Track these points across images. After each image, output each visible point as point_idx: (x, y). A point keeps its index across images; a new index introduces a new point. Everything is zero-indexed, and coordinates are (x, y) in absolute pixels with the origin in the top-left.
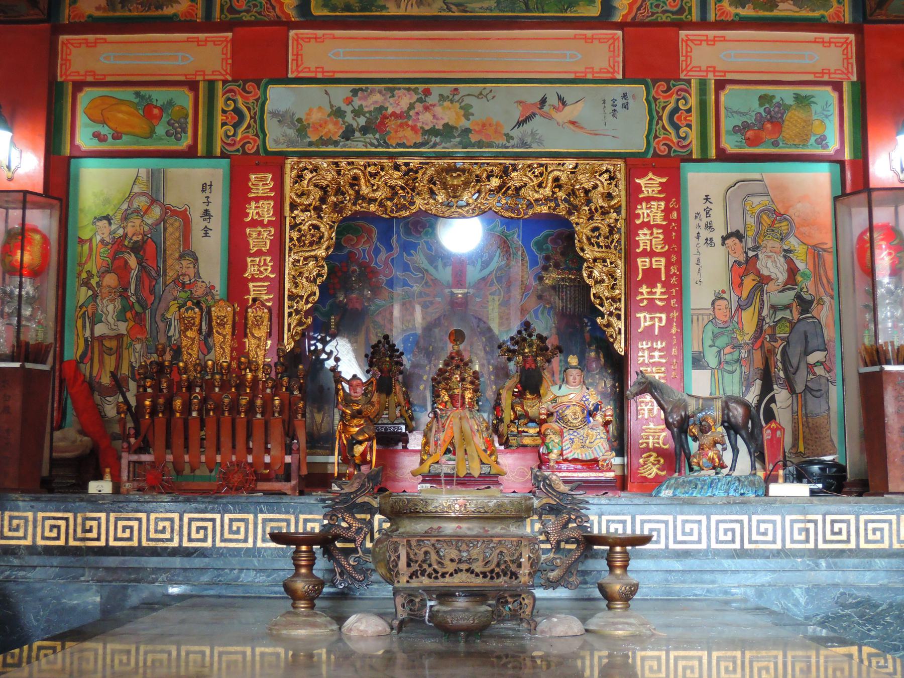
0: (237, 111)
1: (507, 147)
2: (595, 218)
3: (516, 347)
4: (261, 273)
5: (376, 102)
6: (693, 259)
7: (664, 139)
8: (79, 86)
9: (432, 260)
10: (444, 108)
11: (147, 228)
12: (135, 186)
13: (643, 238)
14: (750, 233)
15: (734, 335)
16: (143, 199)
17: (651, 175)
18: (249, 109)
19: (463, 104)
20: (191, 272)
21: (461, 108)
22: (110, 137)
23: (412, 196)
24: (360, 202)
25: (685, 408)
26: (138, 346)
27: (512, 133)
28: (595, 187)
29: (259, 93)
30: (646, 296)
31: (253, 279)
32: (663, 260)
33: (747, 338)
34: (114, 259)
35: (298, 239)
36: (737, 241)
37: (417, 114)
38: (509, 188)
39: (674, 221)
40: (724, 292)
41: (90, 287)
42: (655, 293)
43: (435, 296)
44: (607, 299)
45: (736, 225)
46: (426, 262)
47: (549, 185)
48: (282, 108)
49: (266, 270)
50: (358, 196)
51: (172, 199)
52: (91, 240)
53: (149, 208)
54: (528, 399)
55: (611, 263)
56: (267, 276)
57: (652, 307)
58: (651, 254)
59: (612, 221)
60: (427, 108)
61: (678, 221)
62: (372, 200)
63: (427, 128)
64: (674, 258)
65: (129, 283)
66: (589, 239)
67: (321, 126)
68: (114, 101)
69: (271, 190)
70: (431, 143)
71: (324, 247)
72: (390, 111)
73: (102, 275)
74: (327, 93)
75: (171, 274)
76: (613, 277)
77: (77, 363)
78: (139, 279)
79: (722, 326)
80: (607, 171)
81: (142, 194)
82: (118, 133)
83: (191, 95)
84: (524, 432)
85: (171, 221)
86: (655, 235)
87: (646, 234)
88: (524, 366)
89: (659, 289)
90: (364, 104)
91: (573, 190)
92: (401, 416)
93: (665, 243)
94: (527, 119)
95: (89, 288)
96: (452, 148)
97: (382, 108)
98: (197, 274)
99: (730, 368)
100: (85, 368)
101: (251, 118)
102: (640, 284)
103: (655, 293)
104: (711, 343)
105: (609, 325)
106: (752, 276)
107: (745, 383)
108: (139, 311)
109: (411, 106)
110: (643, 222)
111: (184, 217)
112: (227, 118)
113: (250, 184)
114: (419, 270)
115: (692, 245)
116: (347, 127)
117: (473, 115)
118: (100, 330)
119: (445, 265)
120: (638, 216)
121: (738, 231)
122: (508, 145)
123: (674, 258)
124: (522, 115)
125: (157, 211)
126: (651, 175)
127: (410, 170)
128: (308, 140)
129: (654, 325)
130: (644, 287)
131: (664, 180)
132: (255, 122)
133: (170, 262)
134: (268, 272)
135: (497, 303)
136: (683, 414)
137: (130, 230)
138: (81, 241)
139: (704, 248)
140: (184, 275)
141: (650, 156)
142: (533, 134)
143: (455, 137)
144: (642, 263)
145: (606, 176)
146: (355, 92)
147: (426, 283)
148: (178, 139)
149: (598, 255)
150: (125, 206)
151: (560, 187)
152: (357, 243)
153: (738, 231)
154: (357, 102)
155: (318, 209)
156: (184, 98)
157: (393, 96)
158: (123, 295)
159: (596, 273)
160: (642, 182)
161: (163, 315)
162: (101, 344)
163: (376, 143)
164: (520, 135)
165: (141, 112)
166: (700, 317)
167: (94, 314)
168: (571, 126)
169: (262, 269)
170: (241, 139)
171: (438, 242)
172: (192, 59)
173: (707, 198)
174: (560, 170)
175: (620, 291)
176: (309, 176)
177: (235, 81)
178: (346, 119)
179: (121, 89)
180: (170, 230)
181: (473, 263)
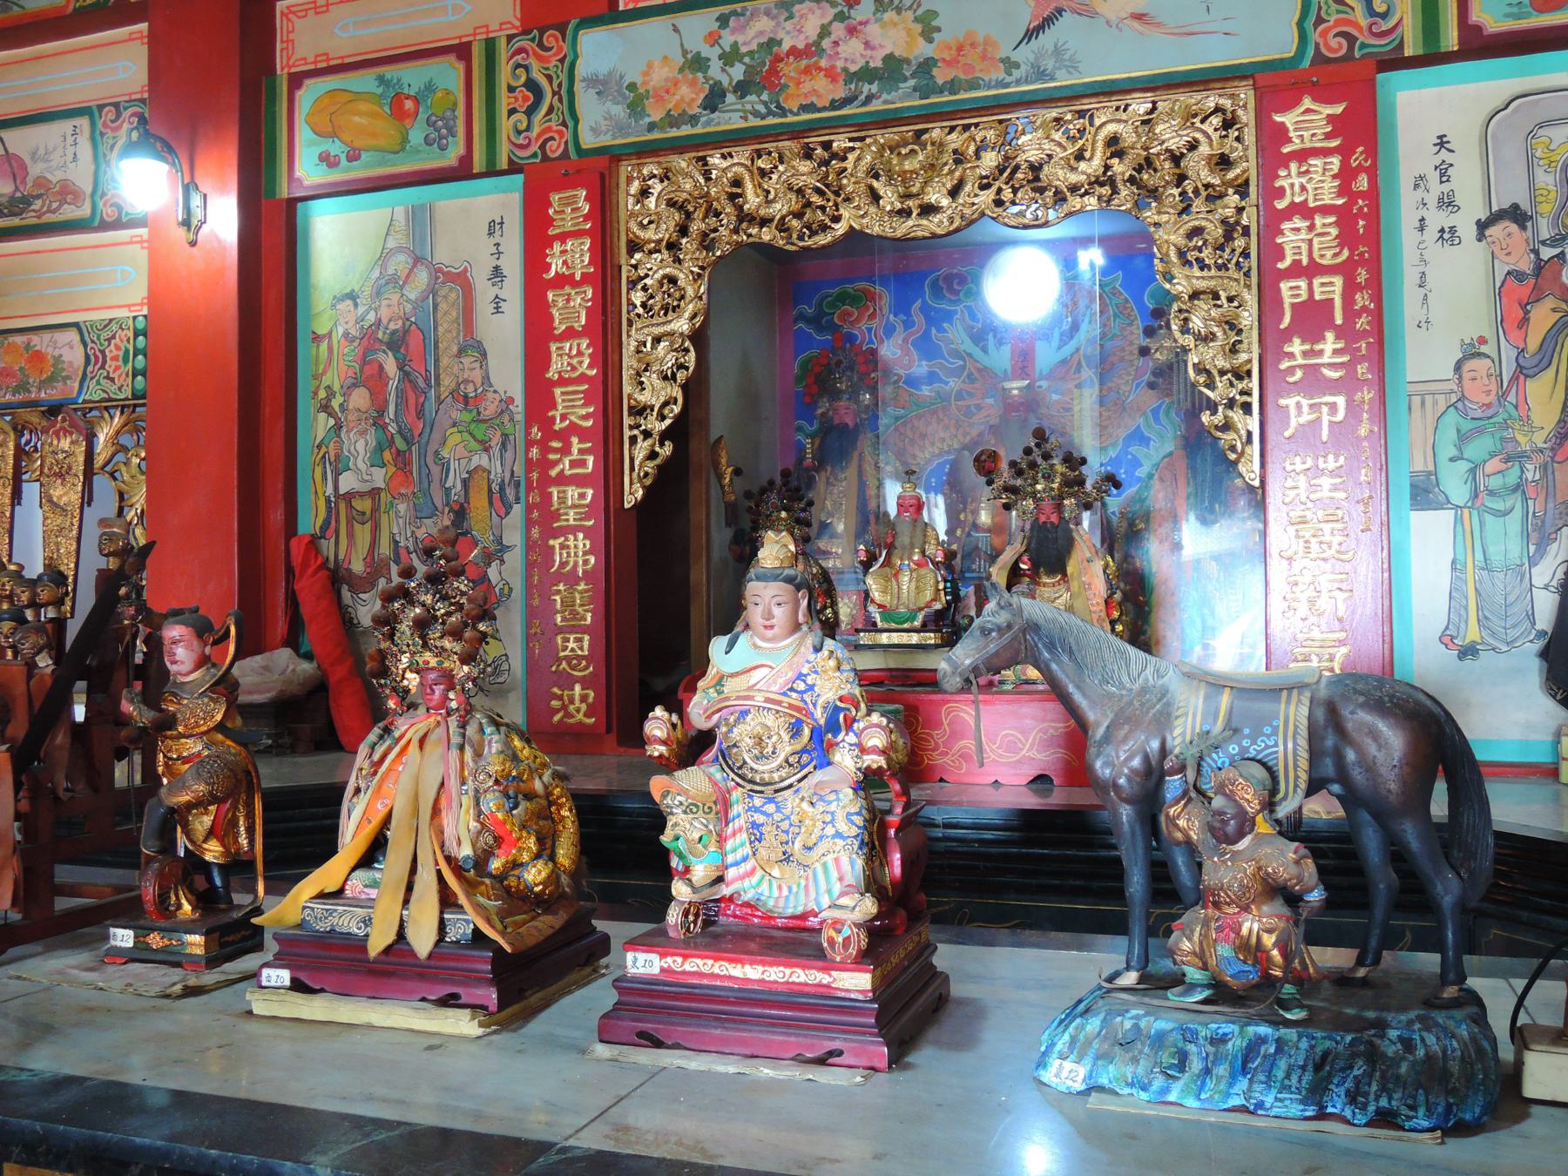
0: (531, 85)
1: (1007, 85)
2: (1194, 209)
3: (1019, 482)
4: (574, 369)
5: (761, 33)
6: (1410, 276)
7: (1338, 23)
8: (296, 81)
9: (978, 338)
10: (884, 26)
11: (409, 307)
12: (390, 238)
13: (1293, 239)
14: (1545, 208)
15: (1508, 434)
16: (402, 258)
17: (1307, 102)
18: (549, 78)
19: (919, 12)
20: (477, 376)
21: (916, 20)
22: (343, 157)
23: (836, 205)
24: (744, 225)
25: (1164, 720)
26: (402, 508)
27: (1016, 56)
28: (1193, 146)
29: (566, 47)
30: (1300, 361)
31: (562, 381)
32: (1338, 281)
33: (1539, 439)
34: (364, 362)
35: (644, 305)
36: (1514, 227)
37: (836, 43)
38: (1017, 168)
39: (1361, 194)
40: (1482, 341)
41: (331, 414)
42: (1321, 352)
44: (1222, 373)
45: (1512, 192)
47: (1099, 154)
48: (603, 70)
49: (581, 363)
50: (744, 217)
51: (444, 255)
52: (330, 334)
53: (411, 270)
54: (1045, 585)
55: (1230, 299)
56: (583, 374)
57: (1314, 382)
58: (1311, 270)
59: (1229, 212)
60: (852, 31)
61: (1373, 195)
62: (765, 222)
63: (853, 68)
64: (1362, 275)
65: (386, 402)
66: (1181, 254)
67: (667, 92)
68: (347, 97)
69: (586, 218)
70: (863, 97)
71: (687, 315)
72: (786, 46)
73: (347, 392)
74: (676, 30)
75: (447, 382)
76: (1232, 326)
77: (313, 541)
78: (401, 395)
79: (1479, 414)
80: (1218, 110)
81: (400, 249)
82: (354, 149)
83: (461, 66)
85: (442, 292)
86: (1319, 230)
87: (1298, 230)
89: (1330, 343)
90: (740, 39)
91: (1147, 159)
93: (1341, 246)
94: (1047, 22)
95: (330, 415)
96: (901, 99)
97: (773, 42)
98: (486, 378)
99: (1499, 505)
100: (328, 547)
101: (554, 94)
102: (1287, 336)
103: (1321, 352)
104: (1453, 452)
105: (1227, 426)
106: (1550, 302)
107: (1534, 536)
108: (404, 453)
109: (825, 31)
110: (1293, 203)
111: (462, 280)
112: (516, 99)
113: (551, 211)
114: (957, 354)
115: (1409, 245)
116: (712, 88)
117: (939, 30)
118: (348, 482)
119: (1000, 343)
120: (1281, 193)
121: (1515, 207)
122: (1009, 79)
123: (1362, 275)
124: (1034, 17)
125: (422, 277)
126: (1307, 102)
127: (834, 156)
128: (647, 120)
129: (1318, 420)
130: (1297, 341)
131: (1338, 109)
132: (560, 100)
133: (444, 361)
134: (585, 367)
136: (1155, 745)
137: (384, 313)
138: (317, 338)
139: (1435, 251)
140: (466, 381)
141: (1306, 63)
142: (1058, 52)
143: (905, 80)
144: (1291, 291)
145: (1216, 121)
146: (723, 21)
147: (969, 376)
148: (443, 148)
149: (1202, 285)
150: (376, 274)
151: (1120, 154)
152: (858, 320)
153: (1515, 207)
154: (727, 39)
155: (672, 246)
156: (448, 75)
157: (791, 17)
158: (378, 423)
159: (1196, 323)
160: (1287, 119)
161: (437, 453)
162: (350, 507)
163: (763, 110)
164: (1032, 58)
165: (387, 109)
166: (1429, 399)
167: (337, 456)
168: (1136, 24)
169: (575, 361)
170: (539, 136)
172: (468, 8)
173: (1442, 142)
174: (1119, 121)
175: (1250, 354)
176: (656, 187)
177: (526, 32)
178: (711, 73)
179: (342, 76)
180: (443, 307)
181: (1047, 337)
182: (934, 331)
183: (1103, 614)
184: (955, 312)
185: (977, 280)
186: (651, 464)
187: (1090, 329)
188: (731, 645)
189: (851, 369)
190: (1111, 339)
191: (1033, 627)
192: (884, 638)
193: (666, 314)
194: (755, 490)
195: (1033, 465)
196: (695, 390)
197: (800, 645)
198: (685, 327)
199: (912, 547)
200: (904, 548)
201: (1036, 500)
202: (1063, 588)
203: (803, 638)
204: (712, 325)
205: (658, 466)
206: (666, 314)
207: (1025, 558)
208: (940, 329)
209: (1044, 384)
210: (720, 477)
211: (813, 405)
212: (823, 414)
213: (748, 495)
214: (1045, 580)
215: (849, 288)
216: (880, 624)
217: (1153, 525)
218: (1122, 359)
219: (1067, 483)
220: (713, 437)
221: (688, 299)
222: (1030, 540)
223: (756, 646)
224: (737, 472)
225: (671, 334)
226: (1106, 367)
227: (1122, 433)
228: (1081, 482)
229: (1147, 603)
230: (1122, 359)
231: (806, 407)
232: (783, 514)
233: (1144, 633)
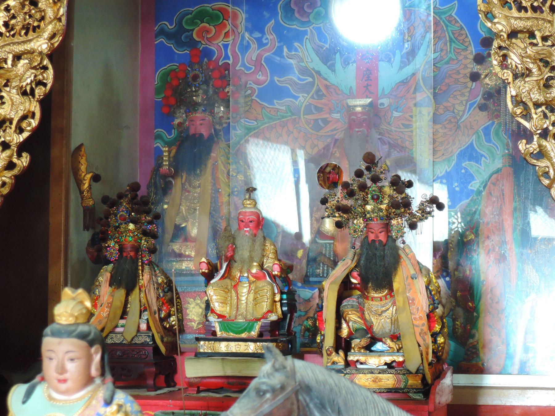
3: (349, 202)
43: (331, 111)
44: (537, 105)
46: (316, 59)
55: (545, 39)
71: (46, 35)
88: (367, 237)
92: (149, 328)
105: (541, 154)
114: (305, 71)
119: (346, 63)
149: (519, 25)
159: (514, 59)
171: (332, 28)
183: (426, 328)
184: (305, 33)
186: (9, 174)
187: (423, 61)
188: (28, 394)
189: (206, 82)
190: (447, 63)
191: (306, 388)
192: (223, 347)
193: (26, 34)
194: (114, 196)
195: (363, 187)
196: (54, 105)
197: (91, 398)
198: (45, 46)
199: (251, 259)
200: (243, 262)
201: (366, 220)
202: (389, 302)
203: (95, 392)
204: (76, 43)
205: (16, 177)
206: (26, 34)
207: (355, 274)
209: (385, 101)
210: (79, 183)
211: (171, 115)
212: (180, 124)
213: (105, 200)
214: (373, 294)
215: (208, 7)
216: (219, 334)
217: (481, 238)
218: (457, 81)
219: (394, 205)
220: (74, 144)
221: (47, 20)
222: (360, 255)
223: (51, 398)
224: (96, 178)
225: (31, 52)
226: (440, 89)
227: (456, 150)
228: (407, 204)
229: (475, 309)
230: (457, 81)
231: (165, 116)
232: (131, 226)
233: (473, 336)
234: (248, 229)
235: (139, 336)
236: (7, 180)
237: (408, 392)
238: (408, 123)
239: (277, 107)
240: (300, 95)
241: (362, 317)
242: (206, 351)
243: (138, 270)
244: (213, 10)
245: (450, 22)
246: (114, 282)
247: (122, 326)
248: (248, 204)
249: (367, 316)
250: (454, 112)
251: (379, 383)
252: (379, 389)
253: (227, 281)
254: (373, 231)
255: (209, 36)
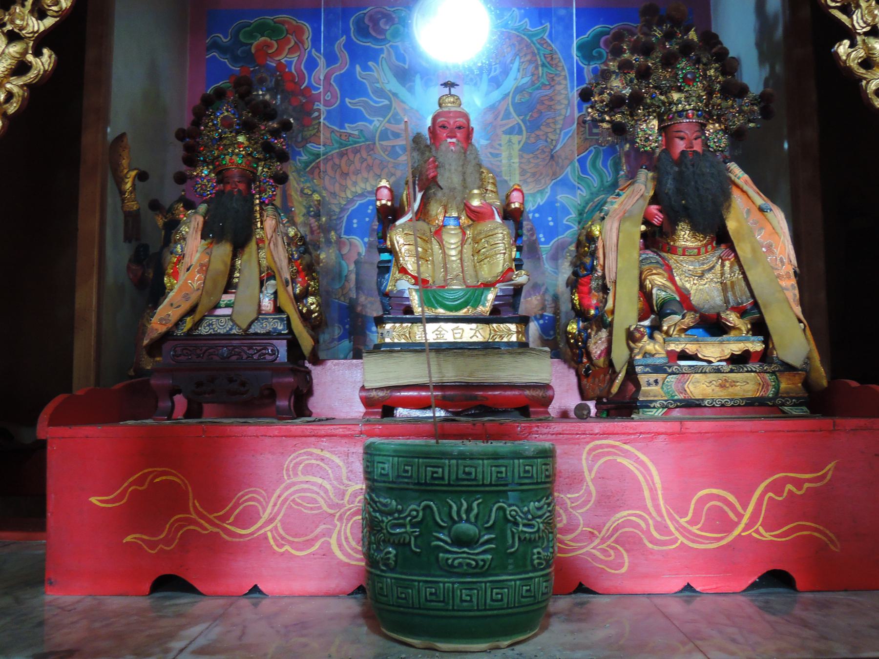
54: (685, 251)
84: (684, 356)
92: (278, 310)
135: (517, 147)
171: (414, 47)
182: (358, 68)
185: (404, 23)
186: (14, 85)
205: (29, 86)
208: (366, 68)
210: (119, 181)
215: (269, 19)
216: (418, 310)
220: (111, 132)
224: (142, 176)
234: (454, 140)
235: (263, 319)
236: (16, 90)
237: (783, 404)
238: (498, 152)
239: (349, 131)
240: (375, 119)
241: (672, 279)
242: (396, 341)
243: (254, 212)
244: (275, 23)
245: (542, 45)
246: (211, 232)
247: (227, 306)
248: (449, 102)
249: (679, 283)
250: (547, 141)
251: (731, 390)
252: (731, 400)
253: (421, 224)
254: (682, 134)
255: (270, 52)
